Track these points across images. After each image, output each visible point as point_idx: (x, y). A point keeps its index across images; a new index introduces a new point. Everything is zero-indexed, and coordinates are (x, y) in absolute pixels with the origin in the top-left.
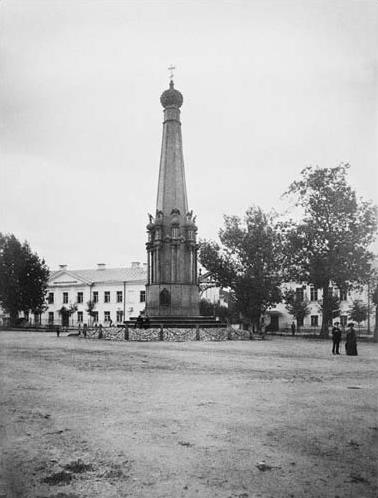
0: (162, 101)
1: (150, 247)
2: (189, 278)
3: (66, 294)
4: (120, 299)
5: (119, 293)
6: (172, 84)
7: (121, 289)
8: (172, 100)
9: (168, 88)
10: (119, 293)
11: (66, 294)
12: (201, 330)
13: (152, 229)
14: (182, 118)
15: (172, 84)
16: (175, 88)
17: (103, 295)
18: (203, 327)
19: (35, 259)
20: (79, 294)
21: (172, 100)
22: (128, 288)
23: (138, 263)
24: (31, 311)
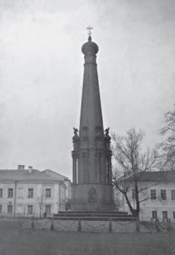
0: (83, 45)
1: (75, 155)
2: (76, 182)
3: (31, 190)
4: (10, 194)
5: (11, 190)
6: (90, 38)
7: (12, 186)
8: (90, 50)
9: (87, 41)
10: (11, 190)
11: (31, 190)
12: (113, 223)
13: (76, 140)
14: (98, 61)
15: (90, 38)
16: (93, 40)
17: (7, 190)
18: (115, 220)
19: (73, 142)
20: (47, 190)
21: (90, 50)
22: (19, 185)
23: (23, 166)
24: (160, 221)
